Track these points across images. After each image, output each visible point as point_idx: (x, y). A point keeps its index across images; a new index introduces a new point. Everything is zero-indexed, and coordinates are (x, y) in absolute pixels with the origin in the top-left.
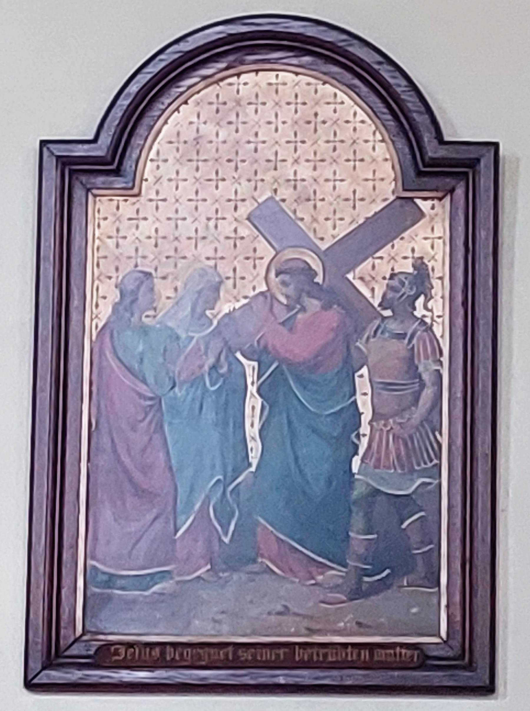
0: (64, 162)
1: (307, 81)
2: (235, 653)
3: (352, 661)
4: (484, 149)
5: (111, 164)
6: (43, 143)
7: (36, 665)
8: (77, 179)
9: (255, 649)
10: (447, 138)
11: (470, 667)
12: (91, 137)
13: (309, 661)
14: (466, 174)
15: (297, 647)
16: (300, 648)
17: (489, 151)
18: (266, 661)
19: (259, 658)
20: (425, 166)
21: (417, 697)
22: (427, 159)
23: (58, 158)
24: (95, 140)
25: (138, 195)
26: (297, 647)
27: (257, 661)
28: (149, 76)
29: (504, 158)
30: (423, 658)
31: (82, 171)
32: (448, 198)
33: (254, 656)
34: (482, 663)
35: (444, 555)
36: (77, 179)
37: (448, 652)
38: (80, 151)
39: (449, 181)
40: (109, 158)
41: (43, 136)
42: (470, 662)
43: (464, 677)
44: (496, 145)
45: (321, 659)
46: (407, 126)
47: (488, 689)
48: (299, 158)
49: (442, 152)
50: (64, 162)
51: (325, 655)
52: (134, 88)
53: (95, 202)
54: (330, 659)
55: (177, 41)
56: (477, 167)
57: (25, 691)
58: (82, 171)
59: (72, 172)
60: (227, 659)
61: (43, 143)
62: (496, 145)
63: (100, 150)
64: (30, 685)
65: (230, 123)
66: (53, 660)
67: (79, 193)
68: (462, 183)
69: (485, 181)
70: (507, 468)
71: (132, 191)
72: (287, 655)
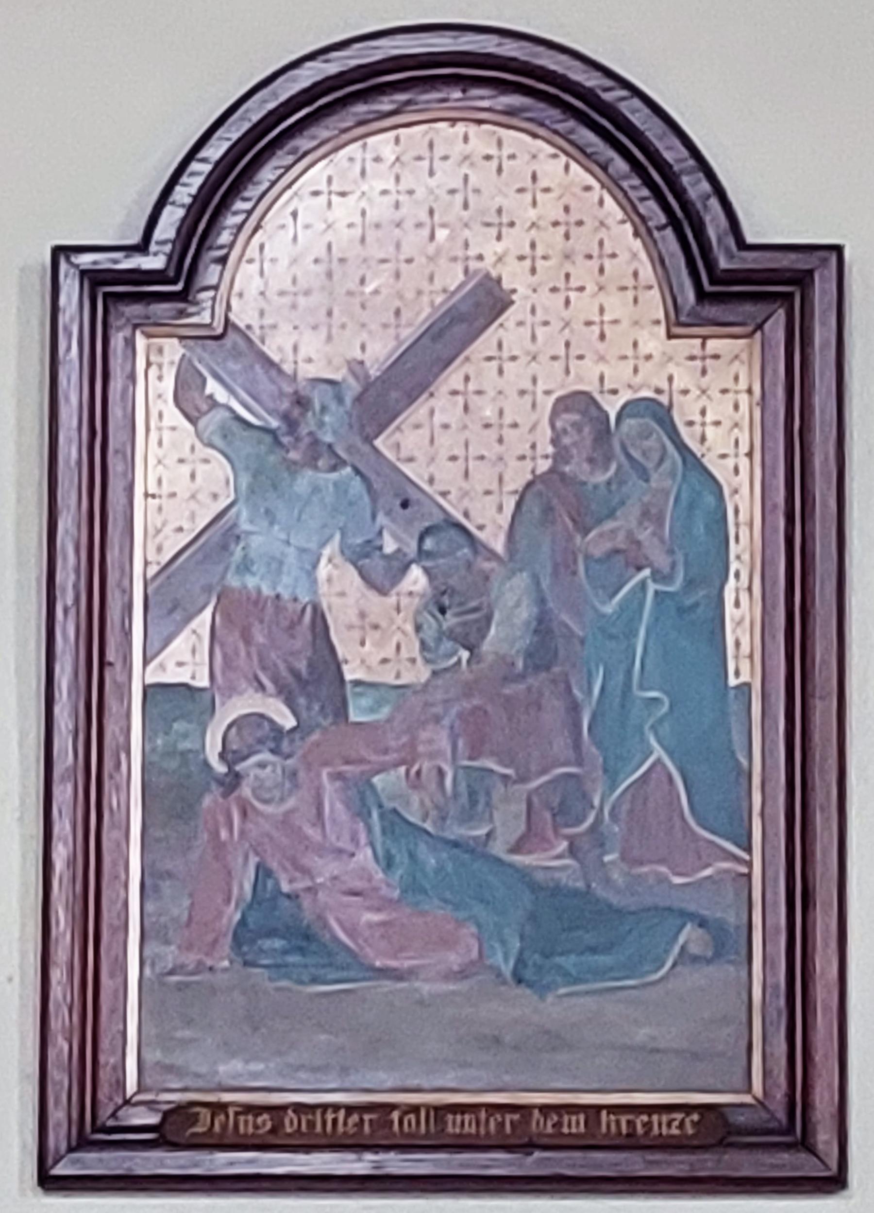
0: (93, 279)
5: (174, 282)
7: (57, 1139)
9: (650, 1115)
10: (750, 239)
13: (628, 1135)
14: (789, 296)
15: (604, 1113)
16: (608, 1113)
17: (825, 261)
18: (410, 1135)
19: (565, 1130)
21: (728, 1198)
23: (83, 273)
28: (226, 145)
30: (716, 1128)
33: (558, 1125)
34: (825, 1137)
35: (826, 945)
40: (171, 273)
42: (792, 1139)
44: (838, 249)
47: (835, 1182)
49: (750, 261)
50: (93, 279)
52: (215, 151)
55: (311, 57)
58: (133, 291)
60: (619, 1133)
62: (838, 249)
64: (48, 1182)
68: (781, 314)
70: (23, 954)
72: (439, 1127)
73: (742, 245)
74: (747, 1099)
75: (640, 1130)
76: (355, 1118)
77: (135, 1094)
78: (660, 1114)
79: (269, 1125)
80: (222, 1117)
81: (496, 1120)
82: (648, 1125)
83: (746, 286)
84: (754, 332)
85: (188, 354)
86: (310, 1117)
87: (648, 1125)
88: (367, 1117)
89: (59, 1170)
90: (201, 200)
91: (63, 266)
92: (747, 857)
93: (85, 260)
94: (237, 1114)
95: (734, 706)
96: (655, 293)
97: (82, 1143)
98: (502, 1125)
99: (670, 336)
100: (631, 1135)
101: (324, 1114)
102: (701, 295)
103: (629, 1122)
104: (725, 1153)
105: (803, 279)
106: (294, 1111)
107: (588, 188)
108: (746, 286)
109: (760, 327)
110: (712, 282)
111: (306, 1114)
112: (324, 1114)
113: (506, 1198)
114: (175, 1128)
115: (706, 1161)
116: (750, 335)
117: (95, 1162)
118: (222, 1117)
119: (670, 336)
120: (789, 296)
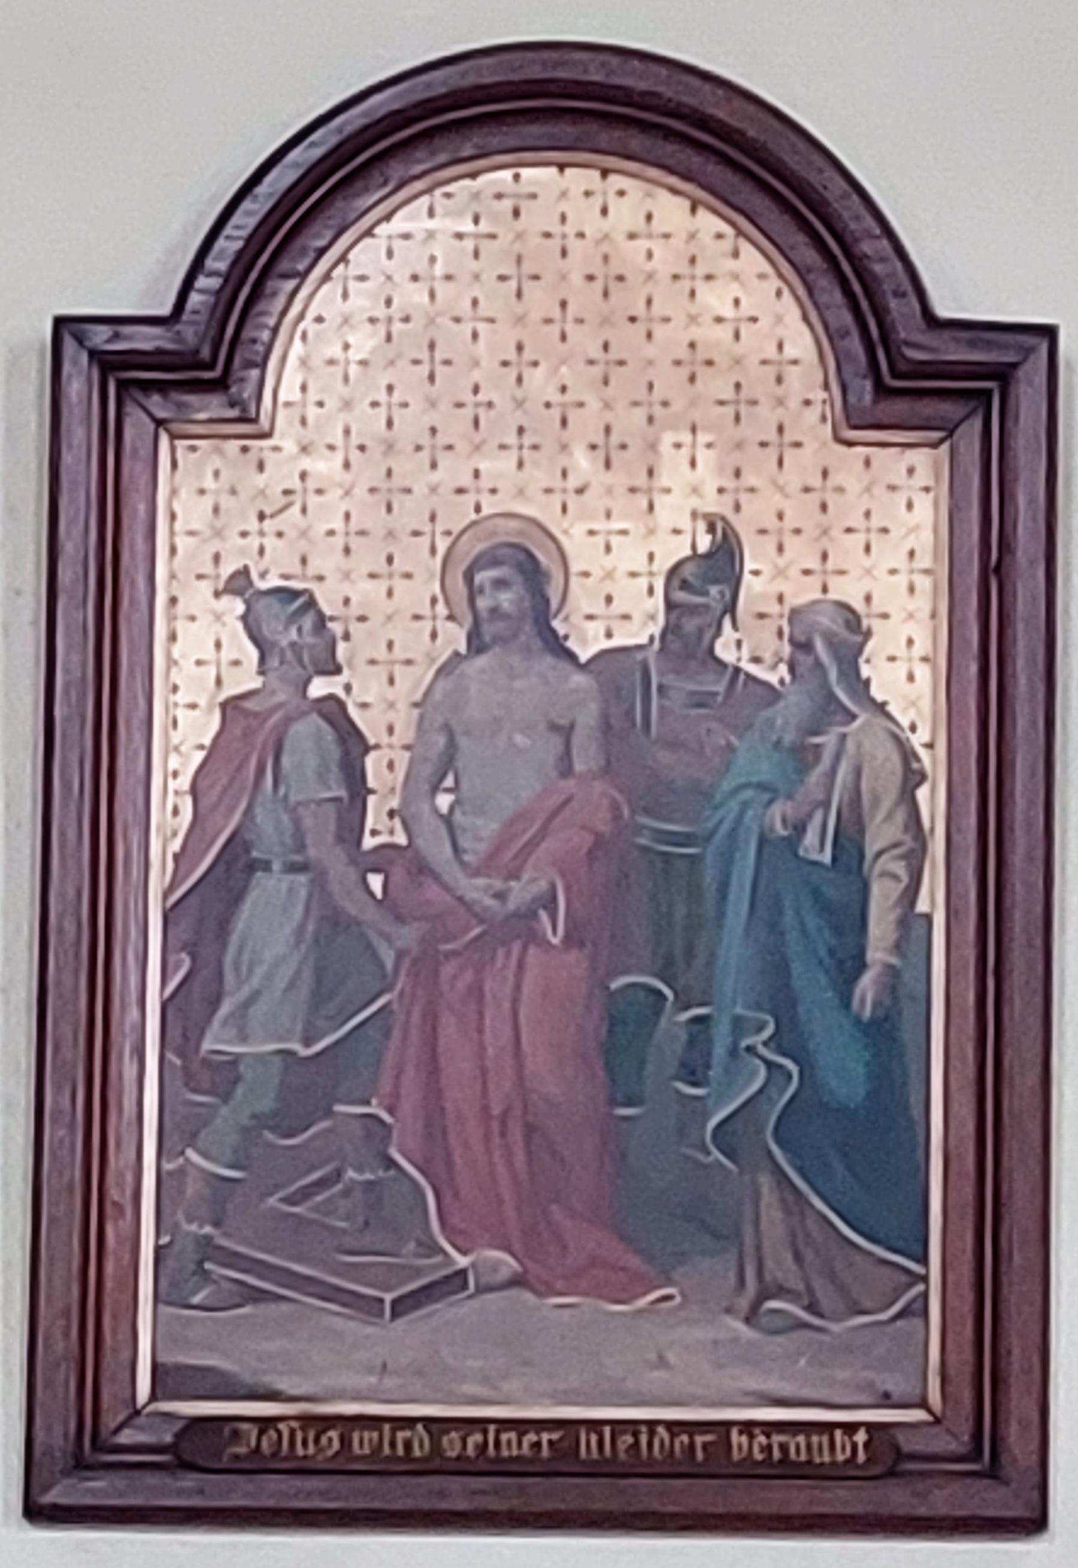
0: (106, 363)
2: (345, 1441)
3: (305, 1457)
4: (1028, 340)
5: (211, 366)
6: (60, 323)
8: (130, 395)
9: (538, 1433)
14: (987, 394)
16: (741, 1433)
18: (511, 1459)
20: (895, 374)
24: (932, 321)
27: (297, 1458)
30: (888, 1456)
31: (170, 367)
32: (945, 447)
36: (130, 395)
37: (948, 1443)
38: (146, 339)
39: (950, 409)
40: (206, 353)
43: (993, 1500)
44: (1049, 333)
45: (400, 1451)
46: (857, 288)
47: (1034, 1523)
50: (106, 363)
53: (173, 450)
57: (25, 1523)
58: (170, 367)
59: (122, 385)
61: (60, 323)
62: (1049, 333)
63: (189, 334)
64: (35, 1512)
67: (136, 426)
71: (247, 421)
74: (918, 1415)
76: (531, 1437)
77: (930, 1411)
78: (362, 1429)
81: (270, 1438)
82: (767, 1449)
83: (915, 368)
84: (942, 441)
85: (720, 699)
86: (375, 1435)
88: (699, 1440)
89: (51, 1497)
90: (243, 261)
91: (69, 345)
94: (498, 1433)
95: (918, 929)
96: (526, 173)
97: (80, 1465)
98: (537, 1445)
100: (785, 1459)
101: (652, 1433)
102: (881, 390)
105: (1004, 374)
107: (719, 236)
108: (915, 368)
109: (951, 434)
111: (402, 1429)
113: (183, 1532)
114: (198, 1448)
116: (935, 445)
117: (97, 1489)
120: (987, 394)
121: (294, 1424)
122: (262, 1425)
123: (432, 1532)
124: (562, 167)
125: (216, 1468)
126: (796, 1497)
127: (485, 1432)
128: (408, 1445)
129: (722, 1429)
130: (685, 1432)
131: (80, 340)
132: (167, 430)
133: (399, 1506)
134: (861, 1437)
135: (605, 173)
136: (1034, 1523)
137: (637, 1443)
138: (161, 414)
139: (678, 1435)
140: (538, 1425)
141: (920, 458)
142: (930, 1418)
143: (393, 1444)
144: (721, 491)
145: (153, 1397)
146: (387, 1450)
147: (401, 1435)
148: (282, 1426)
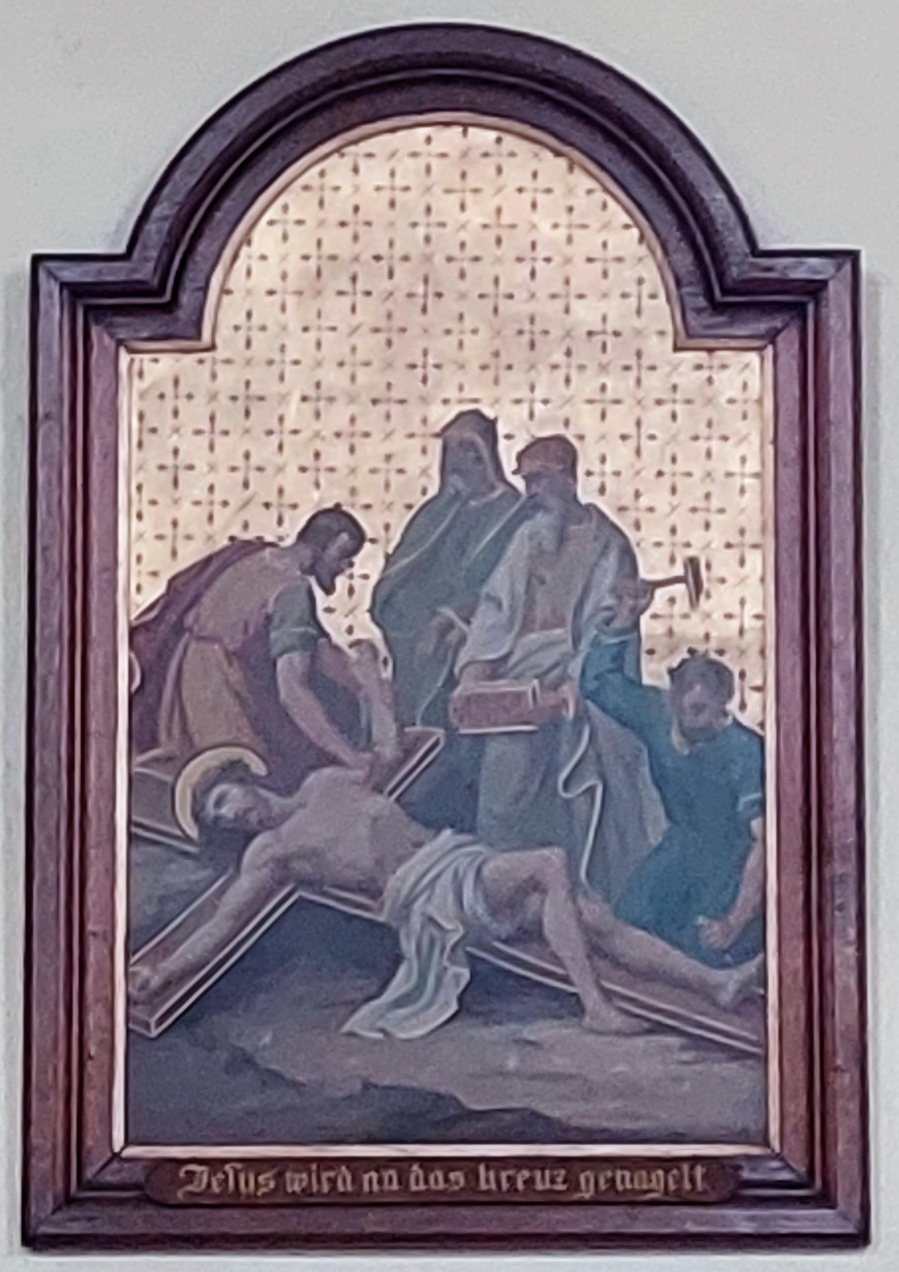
0: (75, 292)
1: (750, 384)
6: (37, 260)
7: (43, 1208)
11: (825, 1199)
12: (121, 249)
14: (803, 306)
15: (482, 1169)
16: (488, 1169)
22: (729, 282)
23: (63, 285)
25: (212, 347)
26: (482, 1169)
29: (873, 283)
30: (727, 1184)
31: (138, 291)
34: (845, 1185)
40: (155, 282)
41: (39, 246)
42: (820, 1184)
44: (853, 256)
47: (858, 1239)
48: (678, 432)
50: (75, 292)
51: (529, 1182)
54: (539, 1187)
56: (824, 294)
57: (25, 1249)
58: (138, 291)
59: (87, 309)
61: (37, 260)
63: (144, 271)
64: (33, 1240)
65: (555, 367)
66: (773, 1150)
69: (836, 318)
73: (756, 252)
75: (520, 1186)
77: (123, 1149)
79: (272, 1185)
80: (221, 1176)
81: (605, 1176)
82: (529, 1182)
83: (738, 284)
87: (612, 1181)
89: (45, 1229)
92: (134, 830)
93: (72, 273)
97: (68, 1201)
98: (511, 1180)
99: (677, 349)
101: (692, 1168)
103: (510, 1179)
104: (541, 1211)
105: (815, 289)
106: (421, 1167)
108: (738, 284)
110: (725, 292)
111: (505, 1169)
112: (692, 1168)
115: (375, 1224)
118: (675, 1172)
119: (677, 349)
121: (239, 1166)
122: (691, 1162)
123: (739, 1252)
124: (465, 126)
125: (155, 1207)
126: (338, 1222)
127: (679, 1169)
128: (333, 1181)
129: (472, 1165)
130: (563, 1167)
131: (51, 274)
132: (126, 347)
133: (500, 1230)
134: (699, 1171)
135: (465, 126)
136: (858, 1239)
137: (226, 1180)
138: (121, 336)
139: (432, 1170)
140: (445, 1164)
141: (753, 358)
142: (117, 1149)
143: (692, 1180)
144: (675, 388)
145: (127, 1143)
146: (687, 1186)
147: (325, 1175)
148: (227, 1167)
